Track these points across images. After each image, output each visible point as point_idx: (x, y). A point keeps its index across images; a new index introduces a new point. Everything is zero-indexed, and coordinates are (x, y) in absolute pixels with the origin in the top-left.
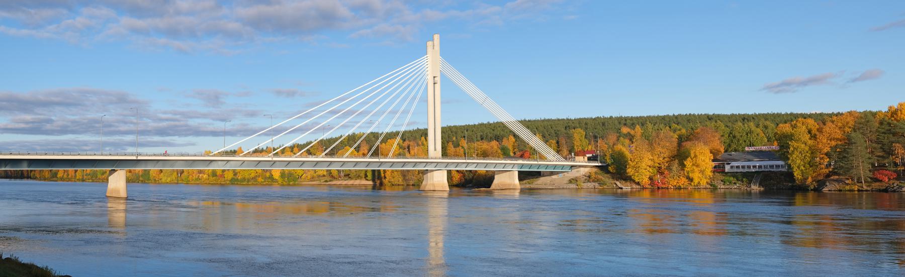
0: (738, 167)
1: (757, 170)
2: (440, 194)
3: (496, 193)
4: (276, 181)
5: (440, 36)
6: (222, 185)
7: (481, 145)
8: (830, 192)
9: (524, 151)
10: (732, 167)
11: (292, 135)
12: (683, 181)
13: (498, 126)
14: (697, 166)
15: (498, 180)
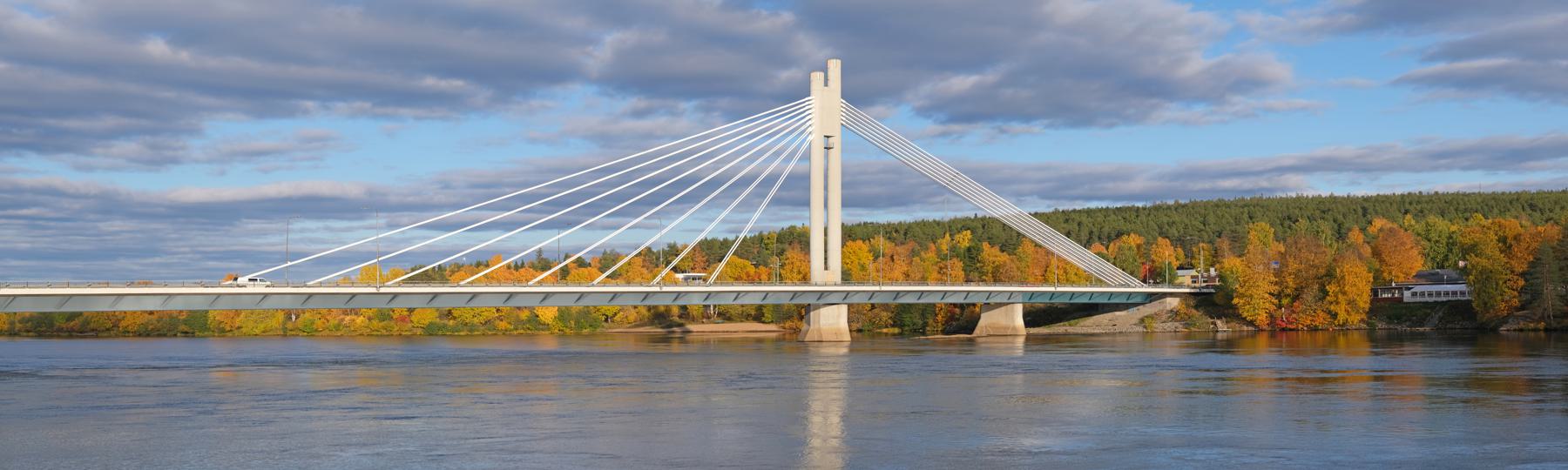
0: (1423, 294)
1: (1450, 298)
2: (832, 350)
3: (983, 345)
4: (546, 326)
5: (814, 71)
6: (409, 338)
7: (996, 256)
8: (1522, 335)
9: (1047, 267)
10: (1414, 294)
11: (539, 233)
12: (1321, 319)
13: (1407, 200)
14: (1344, 293)
15: (987, 320)
